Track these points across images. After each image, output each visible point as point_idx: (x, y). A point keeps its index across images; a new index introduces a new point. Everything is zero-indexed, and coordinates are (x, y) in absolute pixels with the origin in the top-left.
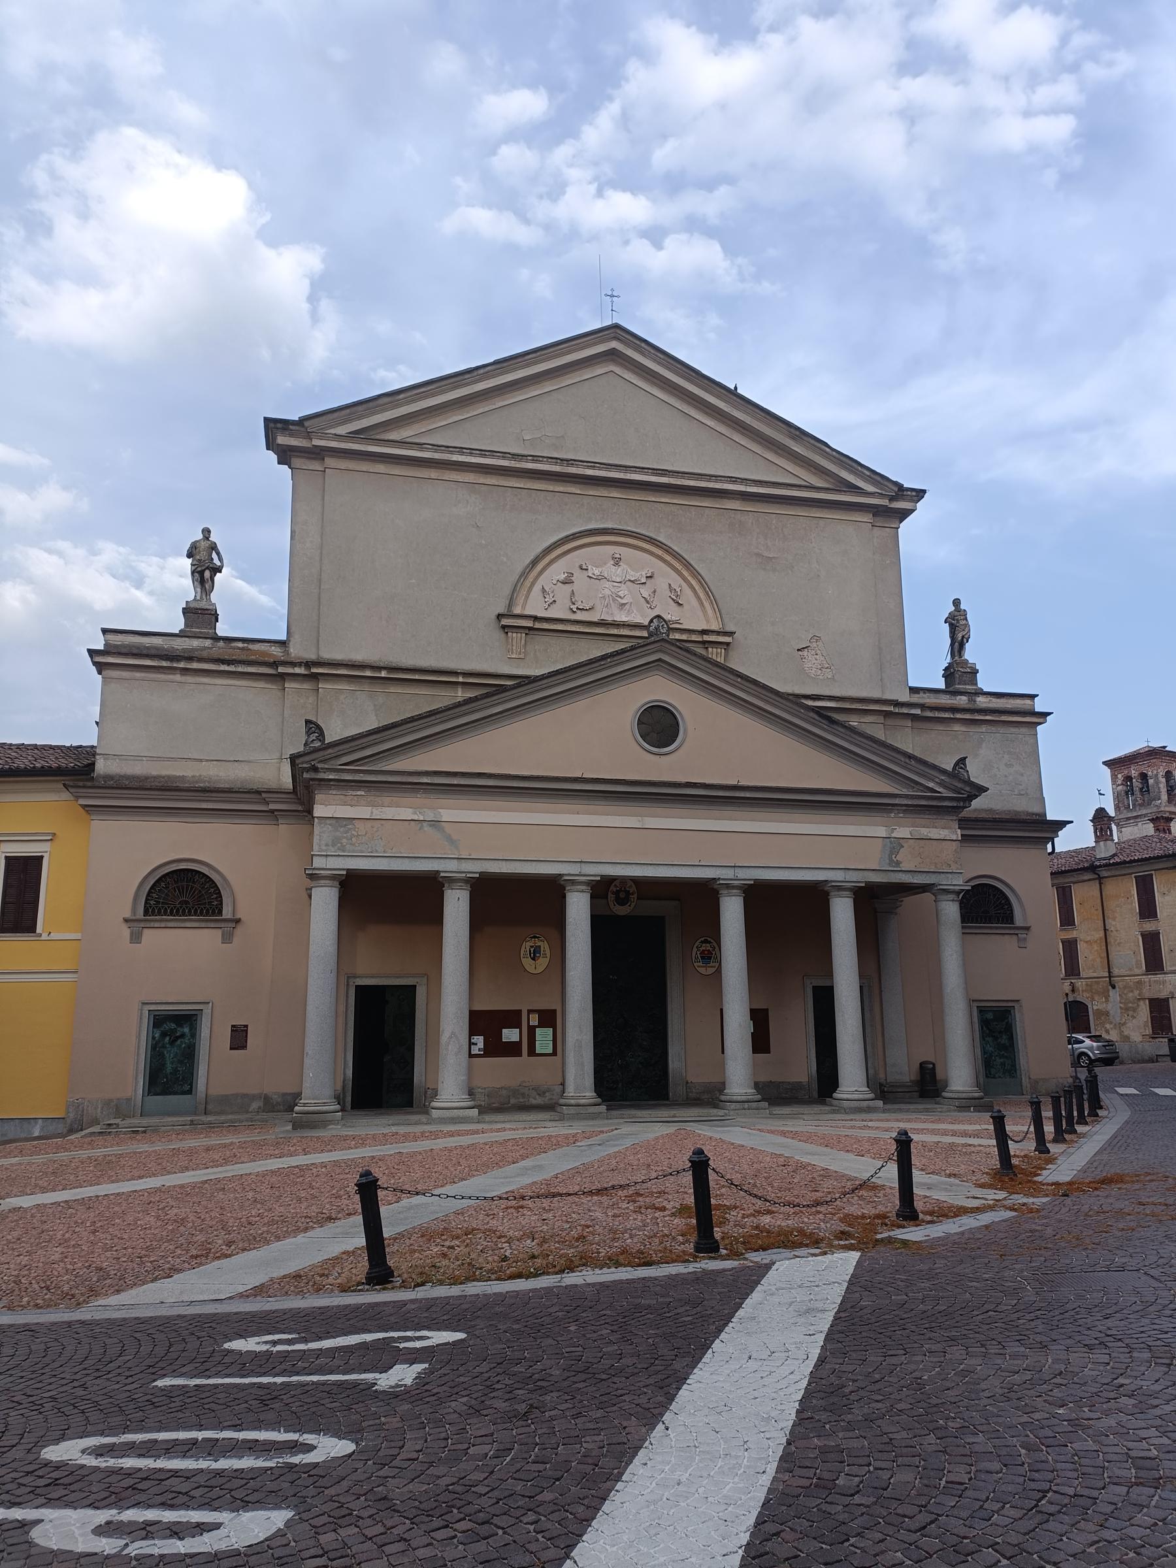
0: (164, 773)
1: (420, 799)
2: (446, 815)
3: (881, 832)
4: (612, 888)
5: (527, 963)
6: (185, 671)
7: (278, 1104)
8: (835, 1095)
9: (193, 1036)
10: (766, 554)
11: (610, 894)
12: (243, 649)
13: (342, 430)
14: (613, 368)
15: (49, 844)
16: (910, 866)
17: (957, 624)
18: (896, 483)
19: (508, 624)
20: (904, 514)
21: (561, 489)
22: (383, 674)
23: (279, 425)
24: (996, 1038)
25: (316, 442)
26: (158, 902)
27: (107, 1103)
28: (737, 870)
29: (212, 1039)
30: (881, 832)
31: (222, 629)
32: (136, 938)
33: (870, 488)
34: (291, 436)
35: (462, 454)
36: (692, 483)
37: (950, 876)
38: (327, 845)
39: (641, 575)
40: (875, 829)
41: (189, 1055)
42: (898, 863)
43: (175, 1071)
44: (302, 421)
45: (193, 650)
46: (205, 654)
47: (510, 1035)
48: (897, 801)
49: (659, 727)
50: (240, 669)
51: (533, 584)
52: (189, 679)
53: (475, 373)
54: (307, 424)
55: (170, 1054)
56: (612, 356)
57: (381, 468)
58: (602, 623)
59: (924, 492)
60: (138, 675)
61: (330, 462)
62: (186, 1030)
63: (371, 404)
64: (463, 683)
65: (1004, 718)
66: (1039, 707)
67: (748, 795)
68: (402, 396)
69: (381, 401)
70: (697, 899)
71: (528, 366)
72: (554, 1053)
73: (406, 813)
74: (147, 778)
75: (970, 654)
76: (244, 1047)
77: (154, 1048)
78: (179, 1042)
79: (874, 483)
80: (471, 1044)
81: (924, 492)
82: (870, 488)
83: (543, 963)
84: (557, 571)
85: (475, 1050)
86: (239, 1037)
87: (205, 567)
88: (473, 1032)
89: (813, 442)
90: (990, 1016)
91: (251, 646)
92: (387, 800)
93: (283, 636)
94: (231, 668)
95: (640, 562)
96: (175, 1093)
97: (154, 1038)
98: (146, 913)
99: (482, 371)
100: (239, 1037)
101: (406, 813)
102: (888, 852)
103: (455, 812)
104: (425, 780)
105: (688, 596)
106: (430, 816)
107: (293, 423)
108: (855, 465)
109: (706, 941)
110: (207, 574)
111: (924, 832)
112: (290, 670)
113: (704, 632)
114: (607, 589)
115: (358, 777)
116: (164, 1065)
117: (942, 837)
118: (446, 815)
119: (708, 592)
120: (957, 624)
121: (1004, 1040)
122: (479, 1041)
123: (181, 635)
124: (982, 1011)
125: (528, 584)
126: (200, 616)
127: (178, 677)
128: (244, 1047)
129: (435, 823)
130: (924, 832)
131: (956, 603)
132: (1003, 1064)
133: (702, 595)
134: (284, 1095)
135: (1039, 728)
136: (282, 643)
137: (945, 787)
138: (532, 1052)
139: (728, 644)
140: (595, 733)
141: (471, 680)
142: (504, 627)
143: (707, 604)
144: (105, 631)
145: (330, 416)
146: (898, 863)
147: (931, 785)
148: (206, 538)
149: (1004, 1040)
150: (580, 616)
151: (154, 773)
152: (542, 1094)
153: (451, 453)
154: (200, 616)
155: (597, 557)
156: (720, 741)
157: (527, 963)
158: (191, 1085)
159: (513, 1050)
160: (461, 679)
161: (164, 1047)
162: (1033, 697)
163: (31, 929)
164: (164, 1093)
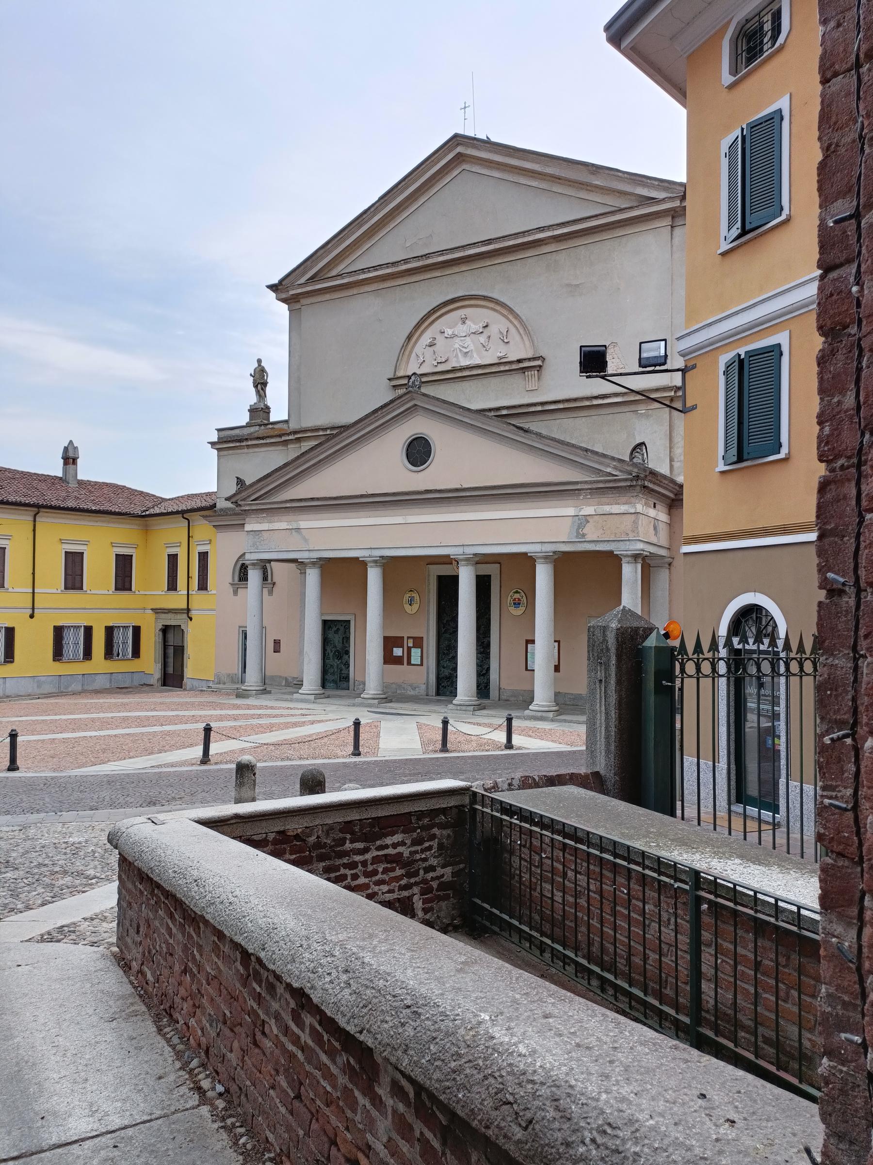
1: (291, 517)
2: (303, 524)
3: (571, 511)
5: (407, 607)
6: (248, 446)
10: (575, 283)
13: (302, 280)
16: (595, 538)
21: (429, 276)
25: (292, 292)
27: (229, 675)
28: (465, 548)
30: (571, 511)
31: (273, 418)
35: (364, 273)
36: (511, 243)
37: (628, 543)
39: (478, 327)
40: (567, 510)
42: (584, 535)
45: (251, 434)
46: (256, 435)
47: (398, 652)
49: (418, 452)
50: (268, 441)
51: (411, 352)
52: (251, 450)
53: (369, 213)
56: (460, 158)
57: (328, 297)
58: (454, 370)
60: (231, 452)
61: (304, 301)
63: (314, 258)
67: (468, 494)
68: (330, 246)
69: (319, 254)
70: (522, 564)
71: (402, 192)
72: (422, 664)
73: (283, 525)
76: (279, 652)
79: (666, 189)
83: (415, 607)
84: (426, 339)
89: (607, 172)
91: (276, 426)
92: (276, 518)
93: (286, 418)
95: (478, 316)
98: (240, 580)
99: (372, 209)
101: (283, 525)
102: (576, 527)
103: (307, 522)
106: (294, 525)
108: (644, 179)
109: (517, 592)
111: (607, 509)
112: (287, 438)
113: (519, 361)
114: (457, 343)
117: (621, 511)
118: (303, 524)
119: (525, 328)
123: (248, 425)
125: (407, 353)
126: (259, 412)
127: (246, 450)
128: (279, 652)
129: (298, 529)
130: (607, 509)
133: (522, 331)
136: (286, 422)
137: (620, 471)
138: (409, 663)
139: (540, 366)
140: (379, 464)
143: (525, 338)
144: (219, 430)
145: (294, 274)
146: (584, 535)
147: (609, 470)
150: (441, 368)
152: (414, 689)
153: (359, 274)
154: (259, 412)
155: (449, 324)
156: (462, 458)
157: (407, 607)
159: (398, 661)
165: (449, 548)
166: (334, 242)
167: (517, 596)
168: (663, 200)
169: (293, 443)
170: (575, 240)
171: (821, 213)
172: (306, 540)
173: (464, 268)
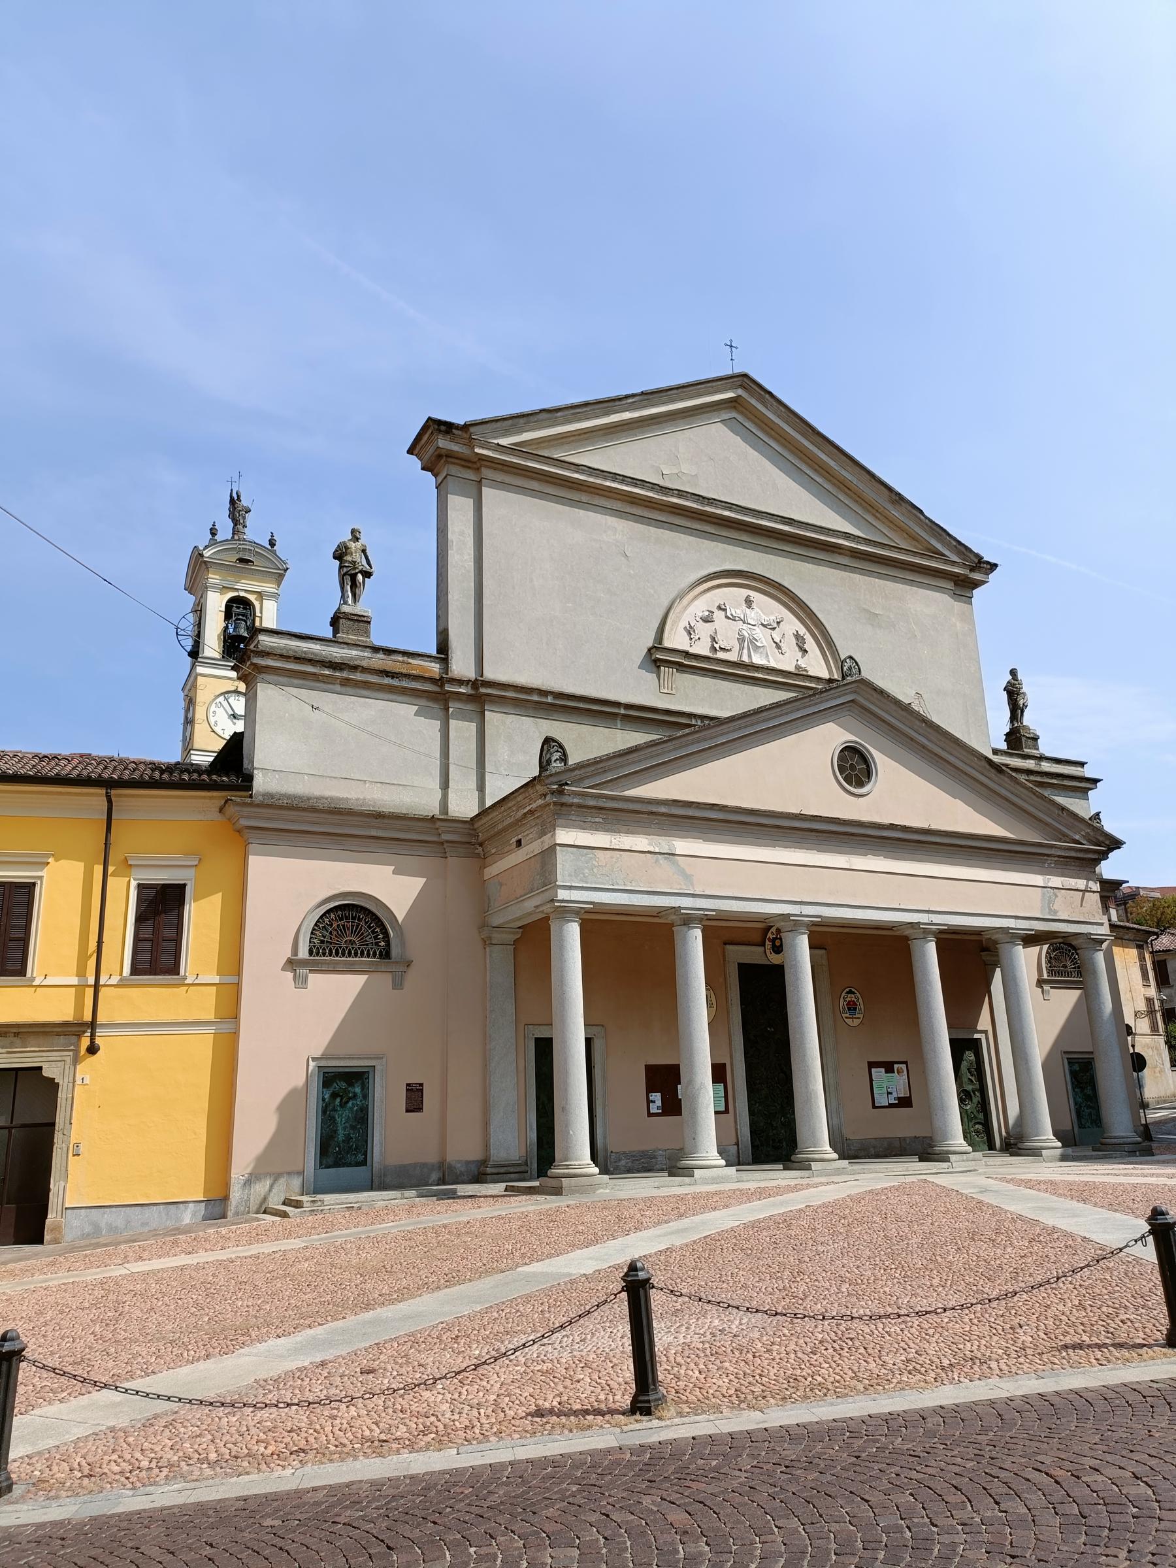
0: (327, 793)
4: (769, 935)
7: (462, 1173)
8: (793, 1158)
9: (366, 1097)
11: (767, 942)
12: (403, 662)
14: (734, 414)
15: (192, 871)
17: (1013, 694)
18: (977, 555)
19: (659, 659)
20: (976, 584)
22: (550, 699)
23: (443, 428)
24: (1083, 1089)
26: (322, 942)
29: (386, 1098)
32: (300, 982)
33: (955, 558)
34: (452, 441)
38: (570, 875)
39: (771, 619)
41: (362, 1119)
42: (1056, 912)
43: (348, 1139)
44: (466, 427)
48: (1052, 852)
49: (854, 768)
50: (404, 684)
54: (472, 429)
55: (343, 1118)
59: (996, 565)
62: (358, 1090)
64: (624, 715)
65: (1066, 783)
66: (1088, 772)
68: (559, 414)
74: (309, 799)
75: (1029, 719)
77: (324, 1112)
78: (350, 1104)
80: (649, 1102)
81: (996, 565)
82: (955, 558)
85: (654, 1110)
86: (415, 1098)
87: (352, 575)
88: (650, 1089)
90: (1076, 1067)
94: (395, 682)
95: (767, 608)
96: (349, 1165)
97: (324, 1100)
100: (415, 1098)
104: (663, 809)
105: (810, 644)
107: (458, 427)
109: (850, 992)
110: (360, 577)
115: (600, 803)
116: (335, 1131)
120: (1013, 694)
121: (1089, 1091)
122: (657, 1097)
124: (1071, 1062)
131: (1013, 673)
132: (1090, 1114)
134: (468, 1163)
135: (1090, 792)
140: (794, 770)
141: (632, 713)
142: (656, 661)
145: (494, 425)
146: (1056, 912)
147: (1077, 837)
148: (356, 539)
149: (1089, 1091)
151: (317, 793)
153: (605, 478)
158: (365, 1154)
160: (622, 711)
161: (334, 1110)
162: (1082, 764)
163: (174, 970)
164: (337, 1164)
165: (921, 915)
166: (566, 412)
167: (851, 998)
168: (953, 563)
169: (459, 700)
170: (868, 563)
171: (226, 628)
172: (688, 878)
173: (745, 538)
